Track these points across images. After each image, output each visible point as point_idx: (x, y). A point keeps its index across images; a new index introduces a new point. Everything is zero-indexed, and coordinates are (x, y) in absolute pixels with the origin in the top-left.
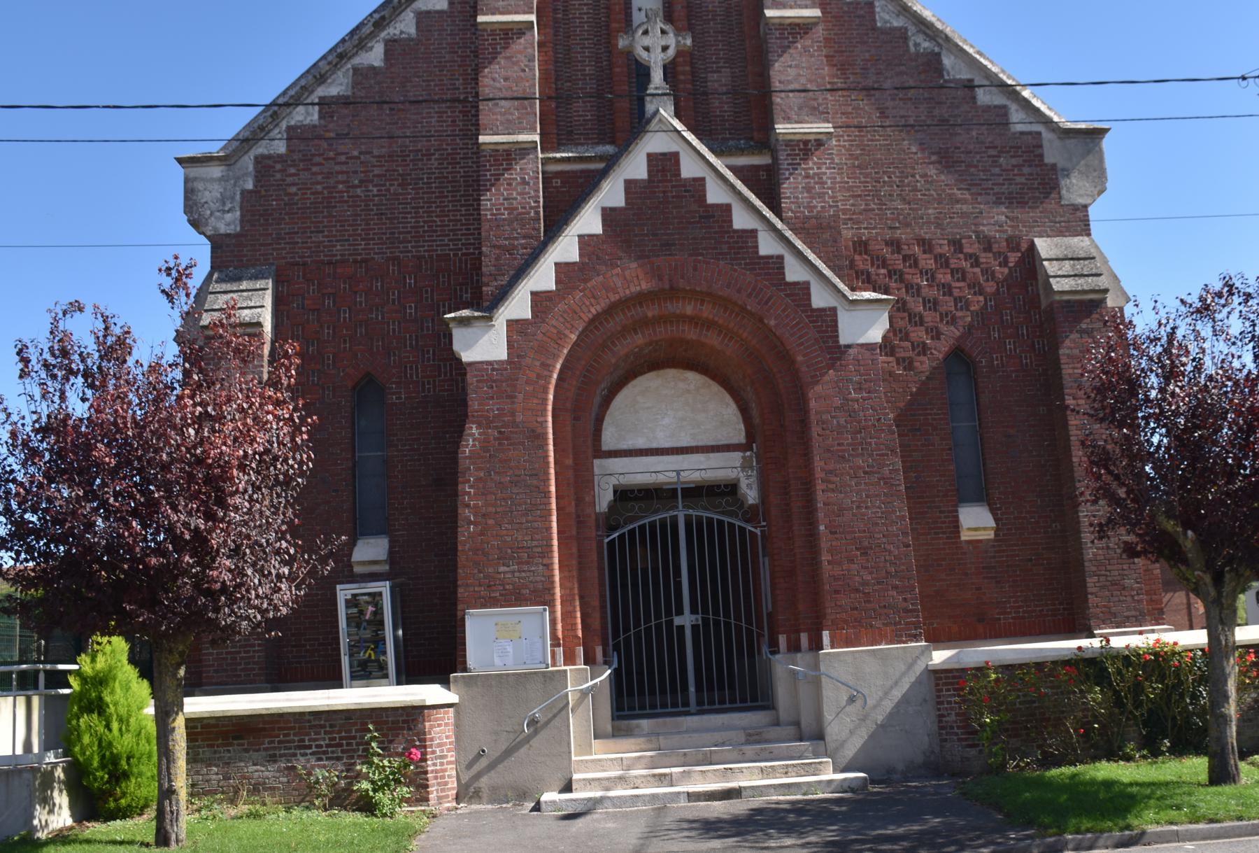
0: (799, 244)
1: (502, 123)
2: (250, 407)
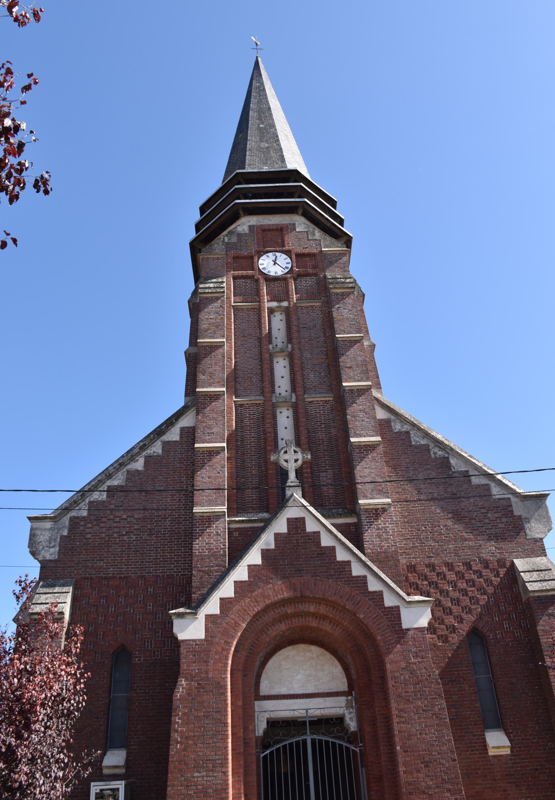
0: (375, 568)
1: (206, 501)
2: (53, 667)
